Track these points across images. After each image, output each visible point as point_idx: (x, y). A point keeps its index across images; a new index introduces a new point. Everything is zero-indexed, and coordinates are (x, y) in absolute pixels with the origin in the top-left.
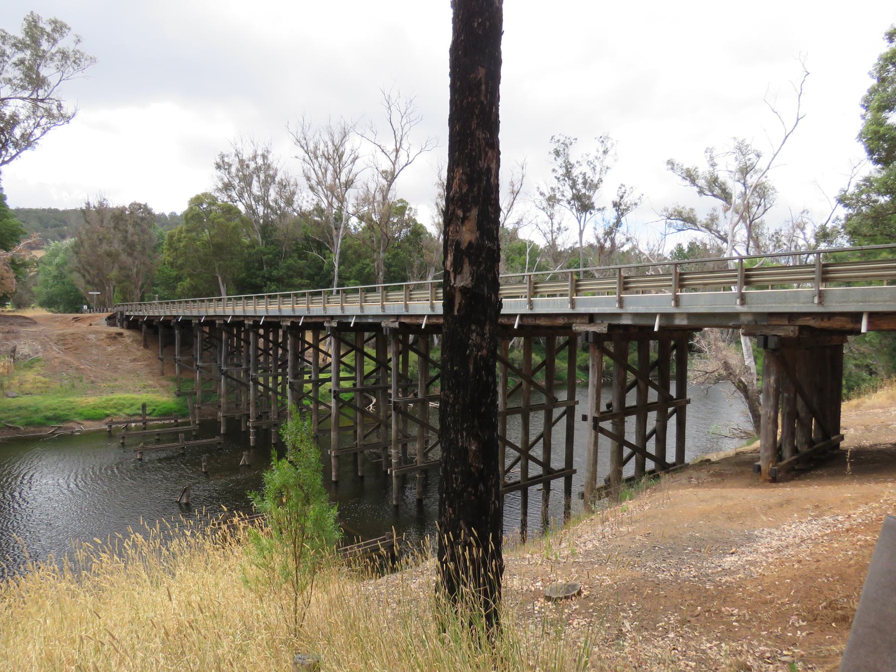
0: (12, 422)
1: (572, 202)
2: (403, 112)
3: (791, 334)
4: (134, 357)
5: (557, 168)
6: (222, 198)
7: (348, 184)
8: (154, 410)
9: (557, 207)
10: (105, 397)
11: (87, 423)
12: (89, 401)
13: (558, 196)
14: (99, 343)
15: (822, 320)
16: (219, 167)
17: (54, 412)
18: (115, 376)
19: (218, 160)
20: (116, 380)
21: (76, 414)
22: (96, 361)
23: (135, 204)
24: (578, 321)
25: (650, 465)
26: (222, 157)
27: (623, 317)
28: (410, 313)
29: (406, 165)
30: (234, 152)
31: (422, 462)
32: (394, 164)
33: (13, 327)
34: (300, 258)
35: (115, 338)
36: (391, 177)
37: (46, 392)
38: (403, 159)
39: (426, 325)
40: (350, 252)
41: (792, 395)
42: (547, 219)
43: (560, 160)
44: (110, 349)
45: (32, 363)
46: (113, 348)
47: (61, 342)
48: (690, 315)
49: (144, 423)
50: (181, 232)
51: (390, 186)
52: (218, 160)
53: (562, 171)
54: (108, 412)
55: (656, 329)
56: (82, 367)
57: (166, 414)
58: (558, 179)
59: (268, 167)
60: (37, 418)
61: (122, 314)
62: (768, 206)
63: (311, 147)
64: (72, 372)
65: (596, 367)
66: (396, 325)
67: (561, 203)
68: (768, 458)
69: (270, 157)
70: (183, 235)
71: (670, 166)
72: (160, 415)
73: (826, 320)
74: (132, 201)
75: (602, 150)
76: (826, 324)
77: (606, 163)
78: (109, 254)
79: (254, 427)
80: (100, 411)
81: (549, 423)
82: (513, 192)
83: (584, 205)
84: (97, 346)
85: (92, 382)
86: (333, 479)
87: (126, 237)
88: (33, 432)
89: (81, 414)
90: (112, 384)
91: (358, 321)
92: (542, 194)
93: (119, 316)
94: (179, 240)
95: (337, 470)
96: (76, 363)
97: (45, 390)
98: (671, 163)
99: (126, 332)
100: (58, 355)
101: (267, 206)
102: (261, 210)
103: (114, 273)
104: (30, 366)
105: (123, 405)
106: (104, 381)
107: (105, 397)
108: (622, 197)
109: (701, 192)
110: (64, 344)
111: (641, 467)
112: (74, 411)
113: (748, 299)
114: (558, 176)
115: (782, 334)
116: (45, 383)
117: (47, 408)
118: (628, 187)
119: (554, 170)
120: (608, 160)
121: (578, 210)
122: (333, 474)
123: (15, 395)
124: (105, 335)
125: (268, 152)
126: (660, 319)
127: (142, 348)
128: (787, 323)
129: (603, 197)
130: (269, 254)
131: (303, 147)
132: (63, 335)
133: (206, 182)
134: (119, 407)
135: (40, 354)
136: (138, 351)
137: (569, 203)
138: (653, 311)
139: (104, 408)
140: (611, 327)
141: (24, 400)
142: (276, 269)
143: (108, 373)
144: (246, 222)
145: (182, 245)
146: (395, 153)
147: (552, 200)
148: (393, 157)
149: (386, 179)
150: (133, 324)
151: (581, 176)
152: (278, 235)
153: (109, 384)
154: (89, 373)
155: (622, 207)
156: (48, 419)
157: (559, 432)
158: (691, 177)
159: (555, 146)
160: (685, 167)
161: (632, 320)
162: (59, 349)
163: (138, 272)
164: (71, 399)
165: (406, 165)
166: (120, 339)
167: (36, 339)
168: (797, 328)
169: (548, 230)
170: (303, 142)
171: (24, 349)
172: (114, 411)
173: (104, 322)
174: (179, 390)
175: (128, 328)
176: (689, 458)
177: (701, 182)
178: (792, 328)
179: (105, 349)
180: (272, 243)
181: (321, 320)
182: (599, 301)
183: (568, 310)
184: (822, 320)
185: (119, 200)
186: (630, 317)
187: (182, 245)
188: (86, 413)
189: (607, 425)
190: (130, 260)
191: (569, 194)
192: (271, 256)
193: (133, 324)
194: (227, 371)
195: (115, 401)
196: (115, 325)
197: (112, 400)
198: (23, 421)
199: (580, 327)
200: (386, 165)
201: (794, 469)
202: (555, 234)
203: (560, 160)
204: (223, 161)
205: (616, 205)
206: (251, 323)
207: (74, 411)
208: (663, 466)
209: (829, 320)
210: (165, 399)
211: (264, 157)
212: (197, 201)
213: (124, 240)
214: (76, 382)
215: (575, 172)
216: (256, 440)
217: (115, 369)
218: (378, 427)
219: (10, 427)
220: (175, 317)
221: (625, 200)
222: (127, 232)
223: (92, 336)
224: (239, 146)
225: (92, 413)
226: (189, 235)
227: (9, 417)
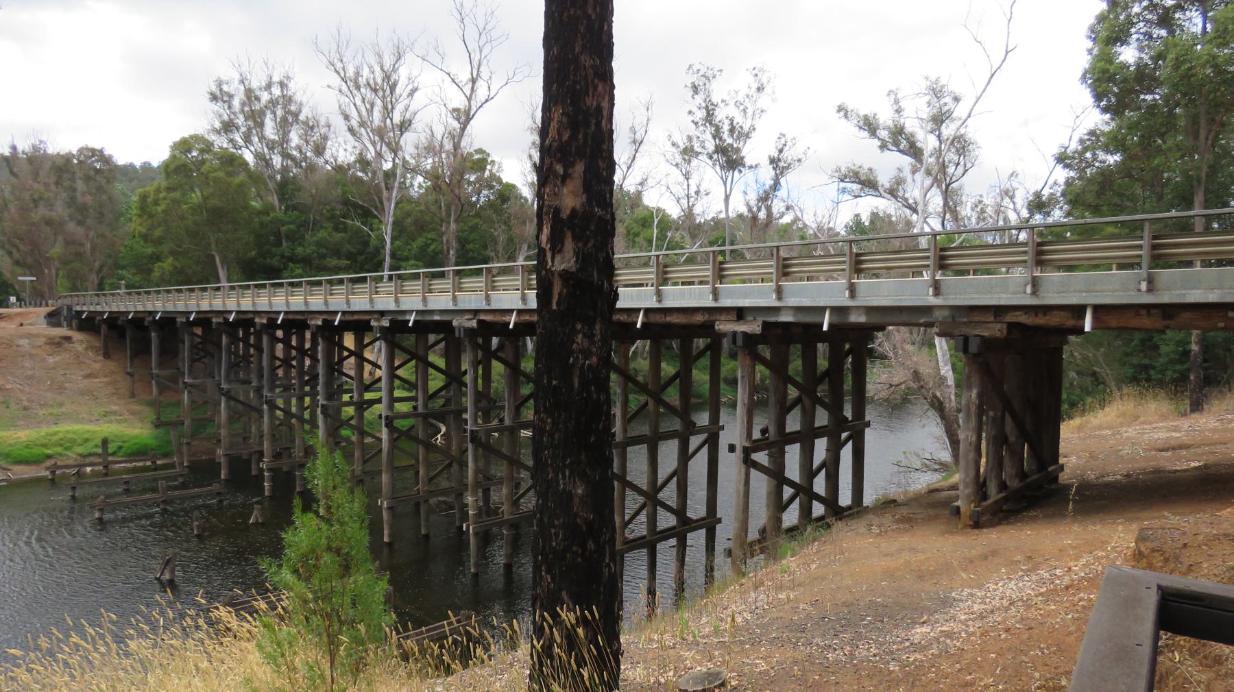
1: (715, 156)
2: (481, 26)
3: (998, 334)
4: (88, 371)
5: (695, 109)
6: (220, 142)
7: (405, 126)
8: (120, 448)
9: (695, 162)
10: (44, 431)
11: (17, 468)
13: (697, 148)
14: (34, 352)
15: (1036, 315)
16: (214, 98)
19: (214, 89)
20: (61, 405)
22: (31, 377)
23: (87, 149)
24: (723, 318)
25: (818, 509)
26: (220, 84)
27: (783, 312)
29: (487, 101)
30: (237, 77)
31: (512, 513)
32: (469, 99)
34: (336, 229)
36: (465, 117)
38: (482, 93)
39: (515, 324)
40: (409, 220)
41: (999, 414)
42: (681, 178)
43: (699, 99)
44: (51, 360)
46: (57, 359)
48: (870, 310)
49: (106, 467)
50: (158, 191)
51: (463, 130)
52: (214, 89)
53: (701, 114)
54: (49, 452)
55: (825, 328)
56: (9, 386)
58: (696, 124)
59: (288, 100)
61: (70, 308)
62: (969, 165)
63: (351, 72)
65: (746, 380)
66: (474, 324)
67: (700, 157)
68: (969, 496)
69: (292, 85)
70: (162, 195)
71: (842, 113)
73: (1040, 315)
74: (81, 146)
75: (754, 86)
76: (1041, 320)
77: (760, 105)
78: (49, 222)
79: (269, 470)
80: (35, 451)
81: (685, 456)
82: (634, 142)
83: (730, 160)
84: (31, 355)
85: (25, 408)
86: (386, 539)
87: (73, 199)
90: (55, 411)
91: (419, 318)
92: (674, 144)
93: (65, 312)
94: (156, 203)
95: (391, 528)
98: (840, 109)
99: (77, 336)
101: (286, 156)
102: (277, 161)
103: (56, 250)
105: (73, 441)
106: (42, 406)
107: (44, 431)
108: (781, 151)
109: (883, 147)
111: (806, 511)
113: (943, 289)
114: (697, 119)
115: (986, 334)
118: (789, 137)
119: (690, 112)
120: (764, 101)
121: (722, 167)
125: (288, 78)
126: (831, 315)
127: (101, 358)
128: (992, 319)
129: (756, 151)
130: (291, 223)
131: (338, 73)
133: (198, 120)
134: (67, 443)
136: (97, 363)
137: (711, 158)
138: (822, 304)
139: (45, 446)
140: (766, 325)
142: (300, 244)
143: (49, 395)
144: (255, 178)
145: (160, 209)
146: (470, 85)
147: (689, 153)
148: (468, 91)
149: (458, 119)
150: (88, 324)
151: (727, 122)
152: (303, 198)
153: (51, 410)
155: (782, 164)
157: (698, 467)
158: (870, 126)
159: (693, 78)
160: (862, 113)
161: (794, 315)
163: (94, 248)
165: (487, 101)
166: (66, 345)
168: (1005, 326)
169: (682, 193)
170: (339, 65)
172: (59, 449)
174: (158, 419)
176: (868, 499)
177: (883, 134)
178: (999, 326)
179: (43, 360)
180: (295, 208)
181: (367, 317)
182: (750, 291)
183: (708, 302)
184: (1036, 315)
185: (64, 143)
186: (791, 312)
187: (160, 209)
189: (762, 457)
190: (80, 231)
191: (711, 145)
192: (292, 227)
193: (88, 324)
194: (229, 391)
195: (61, 435)
196: (58, 325)
197: (56, 433)
199: (725, 326)
200: (459, 101)
201: (1002, 511)
202: (692, 200)
203: (699, 99)
204: (221, 90)
205: (773, 161)
206: (265, 321)
208: (836, 511)
209: (1045, 314)
210: (137, 431)
211: (283, 85)
212: (184, 146)
213: (71, 202)
215: (720, 115)
216: (273, 488)
217: (61, 389)
218: (450, 465)
220: (150, 313)
221: (785, 154)
222: (74, 190)
224: (244, 69)
225: (26, 452)
226: (172, 195)
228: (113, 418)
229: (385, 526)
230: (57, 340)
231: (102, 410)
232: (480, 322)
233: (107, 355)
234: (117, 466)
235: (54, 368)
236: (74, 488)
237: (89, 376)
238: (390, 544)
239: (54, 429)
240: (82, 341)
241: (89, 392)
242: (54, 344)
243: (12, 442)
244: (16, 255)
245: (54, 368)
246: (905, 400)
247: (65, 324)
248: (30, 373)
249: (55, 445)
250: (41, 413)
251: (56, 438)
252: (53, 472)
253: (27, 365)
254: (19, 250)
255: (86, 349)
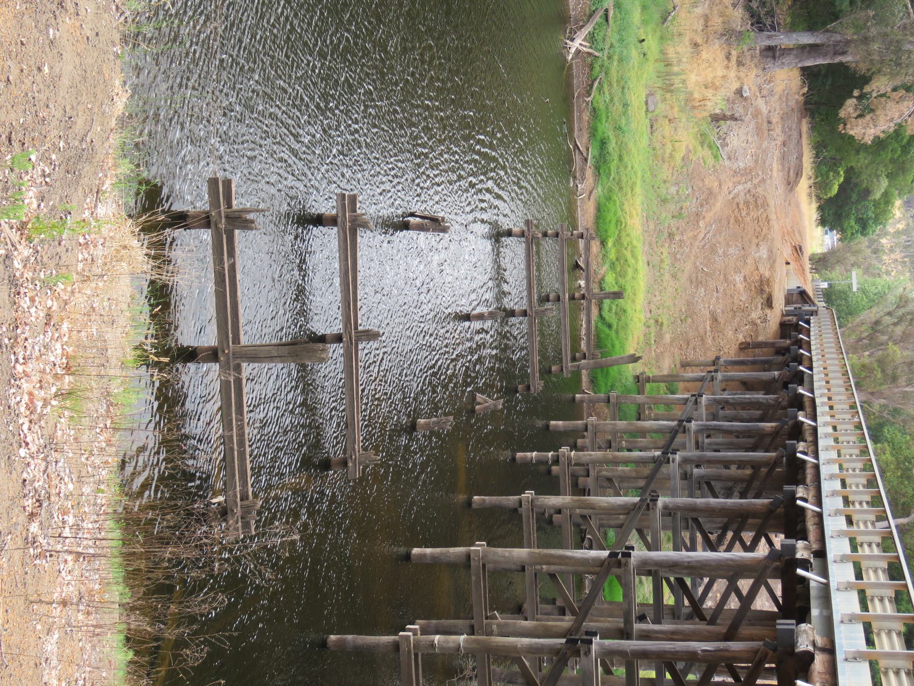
0: (600, 90)
8: (610, 326)
10: (640, 248)
11: (590, 207)
12: (635, 216)
14: (750, 261)
17: (615, 156)
18: (684, 278)
20: (674, 276)
21: (610, 190)
22: (713, 250)
28: (841, 666)
33: (778, 130)
35: (762, 291)
37: (655, 156)
44: (738, 278)
45: (710, 147)
46: (740, 286)
47: (752, 200)
54: (610, 244)
56: (701, 223)
57: (599, 343)
60: (605, 128)
61: (812, 313)
64: (690, 206)
72: (598, 336)
79: (556, 461)
80: (612, 229)
84: (744, 258)
85: (671, 235)
86: (416, 551)
88: (580, 119)
89: (609, 199)
90: (666, 266)
91: (809, 515)
93: (806, 308)
95: (433, 557)
96: (709, 216)
97: (657, 155)
99: (774, 317)
100: (725, 188)
104: (703, 139)
105: (622, 274)
106: (674, 256)
107: (640, 248)
110: (747, 203)
112: (616, 189)
116: (671, 156)
117: (622, 146)
122: (428, 551)
123: (651, 108)
124: (767, 274)
127: (741, 338)
132: (765, 205)
134: (619, 265)
135: (727, 163)
141: (638, 121)
143: (689, 266)
153: (668, 261)
154: (691, 234)
156: (603, 143)
162: (738, 195)
164: (638, 190)
166: (759, 301)
167: (756, 161)
171: (739, 138)
172: (612, 255)
173: (794, 283)
174: (648, 380)
175: (783, 326)
179: (737, 270)
181: (812, 536)
188: (610, 206)
193: (793, 330)
195: (631, 261)
196: (788, 302)
197: (634, 256)
198: (602, 107)
207: (616, 189)
214: (672, 207)
216: (527, 464)
219: (591, 86)
220: (821, 554)
223: (764, 252)
225: (610, 216)
227: (610, 85)
228: (653, 330)
229: (438, 550)
230: (766, 288)
231: (664, 319)
232: (808, 658)
233: (744, 347)
234: (583, 317)
235: (726, 279)
236: (557, 235)
237: (715, 319)
238: (408, 557)
239: (642, 260)
240: (765, 320)
241: (690, 312)
242: (761, 284)
243: (626, 207)
244: (888, 320)
245: (726, 279)
246: (506, 658)
247: (791, 308)
248: (720, 252)
249: (618, 252)
250: (665, 250)
251: (628, 254)
252: (581, 236)
253: (731, 251)
254: (895, 324)
255: (754, 324)
